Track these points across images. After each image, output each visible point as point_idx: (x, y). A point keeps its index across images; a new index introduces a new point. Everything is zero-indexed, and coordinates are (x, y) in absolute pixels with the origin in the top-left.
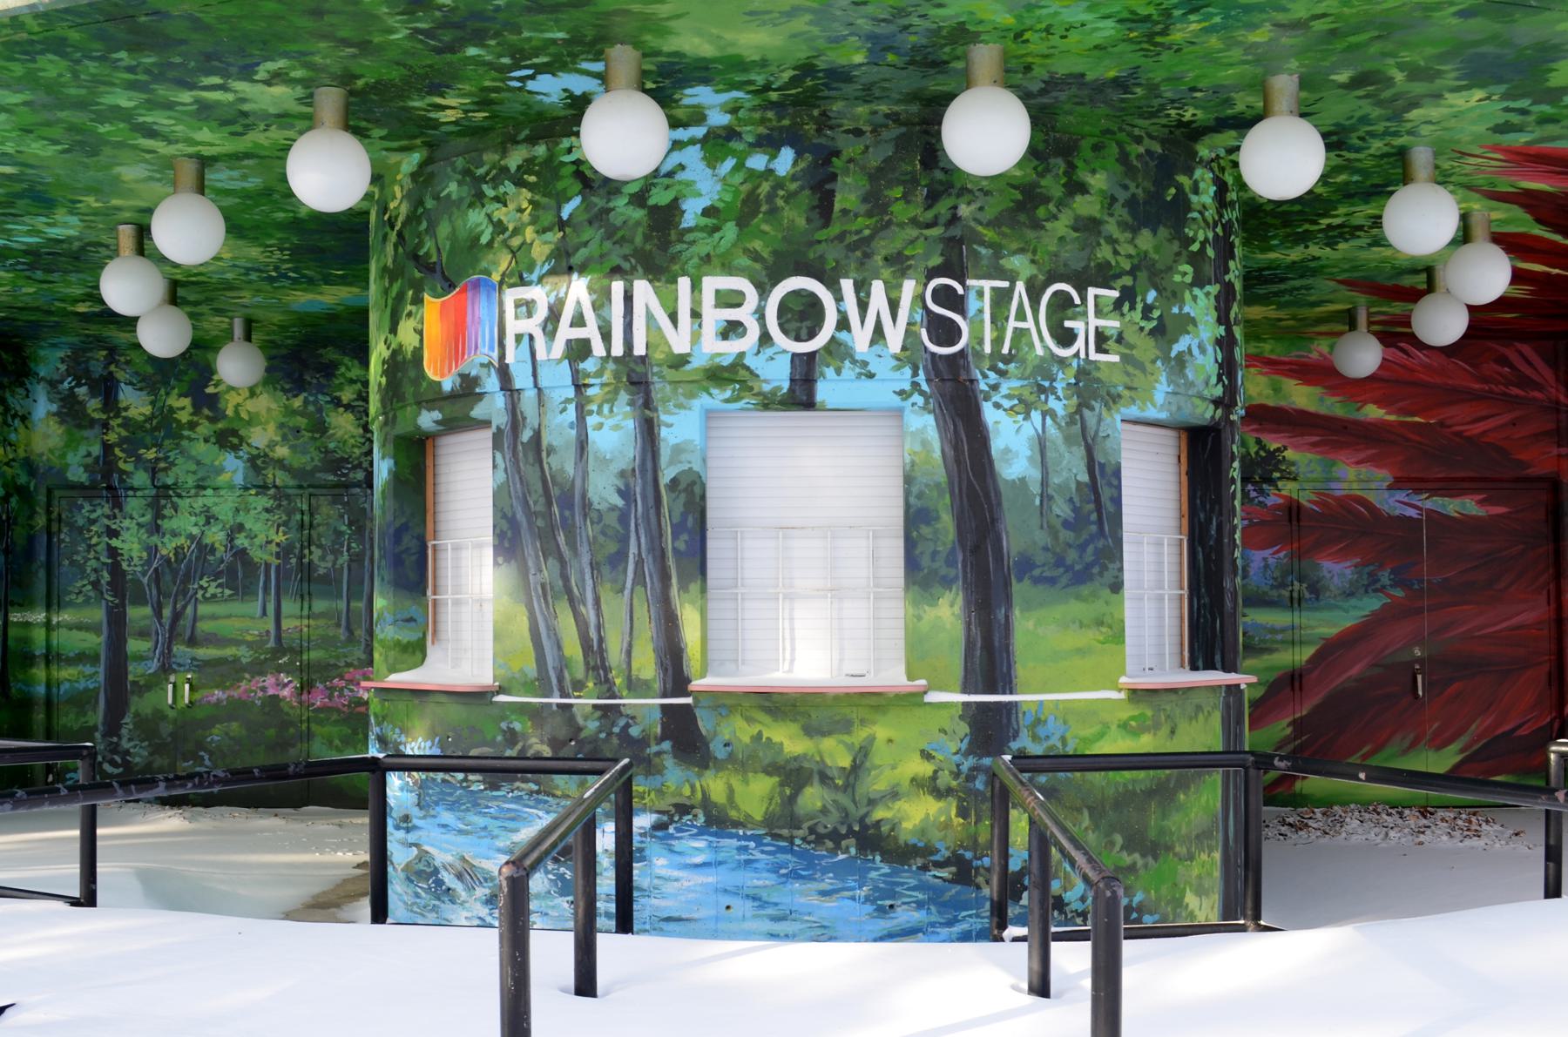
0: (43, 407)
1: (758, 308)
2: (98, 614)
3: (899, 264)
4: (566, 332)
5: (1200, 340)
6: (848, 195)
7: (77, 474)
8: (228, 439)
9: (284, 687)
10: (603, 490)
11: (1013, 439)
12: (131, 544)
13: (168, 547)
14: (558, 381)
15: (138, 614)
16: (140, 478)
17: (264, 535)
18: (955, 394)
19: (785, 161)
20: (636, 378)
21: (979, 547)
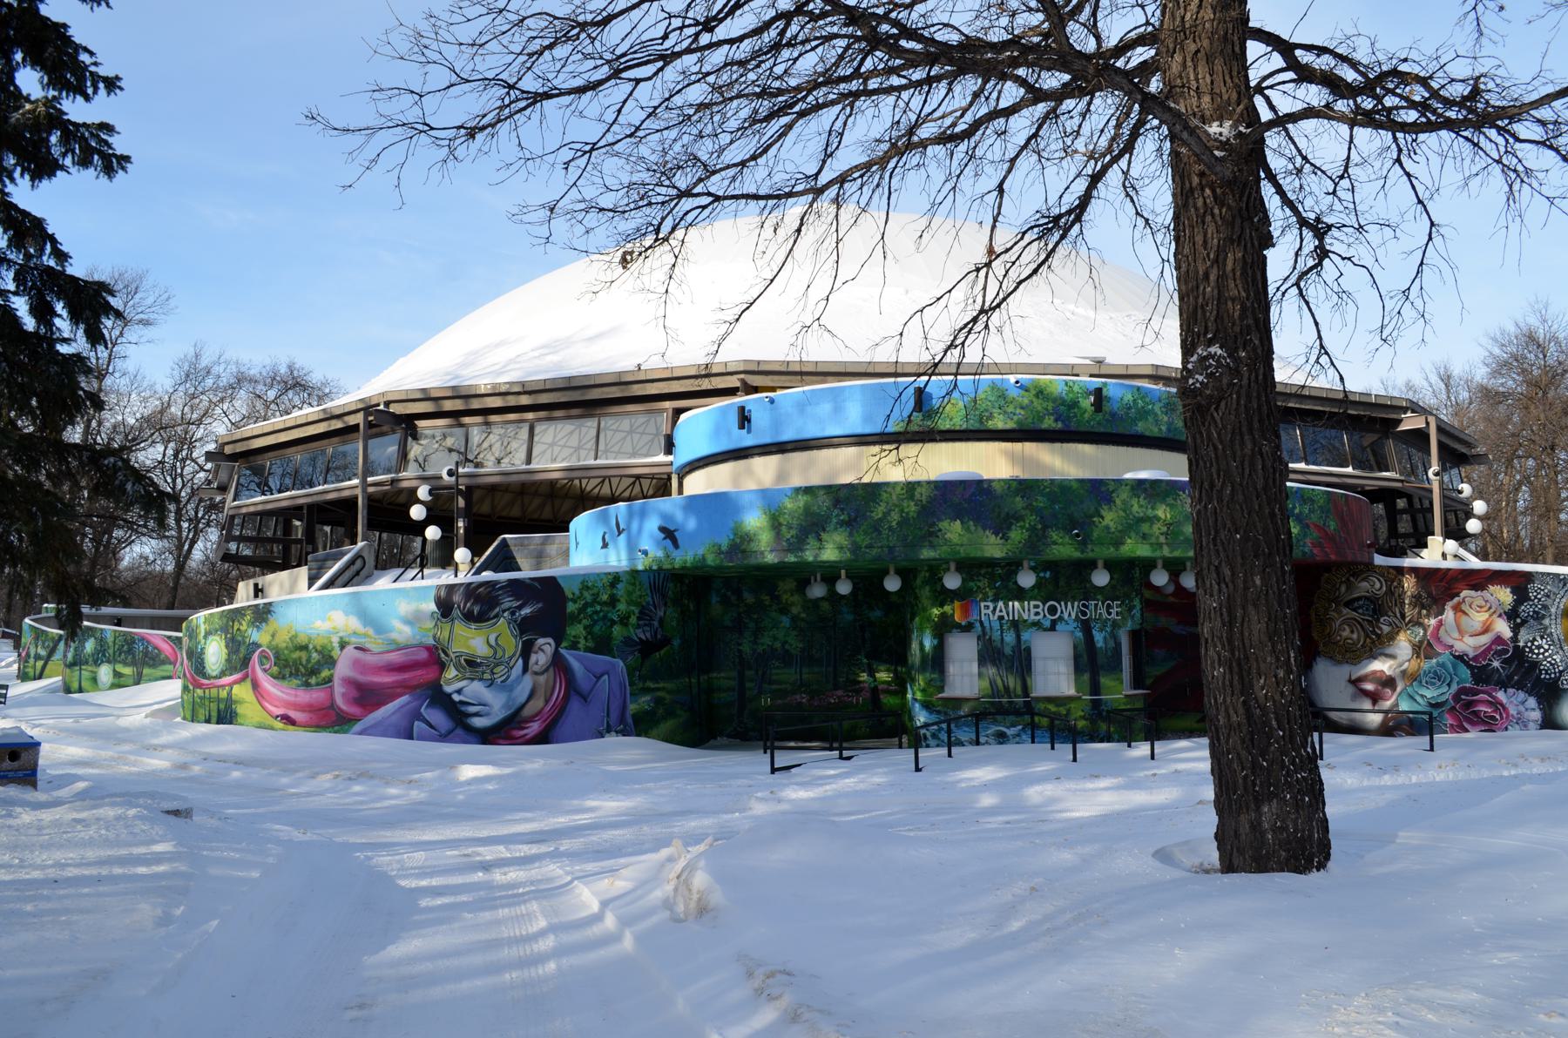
0: (714, 599)
1: (1043, 609)
2: (734, 674)
3: (1074, 599)
4: (998, 613)
5: (1137, 612)
6: (1062, 583)
7: (728, 623)
8: (784, 610)
9: (804, 699)
10: (1008, 651)
11: (1099, 637)
12: (746, 648)
13: (760, 649)
14: (996, 625)
15: (749, 673)
16: (752, 625)
17: (795, 645)
18: (1086, 627)
19: (1048, 574)
20: (1016, 625)
21: (1089, 662)
